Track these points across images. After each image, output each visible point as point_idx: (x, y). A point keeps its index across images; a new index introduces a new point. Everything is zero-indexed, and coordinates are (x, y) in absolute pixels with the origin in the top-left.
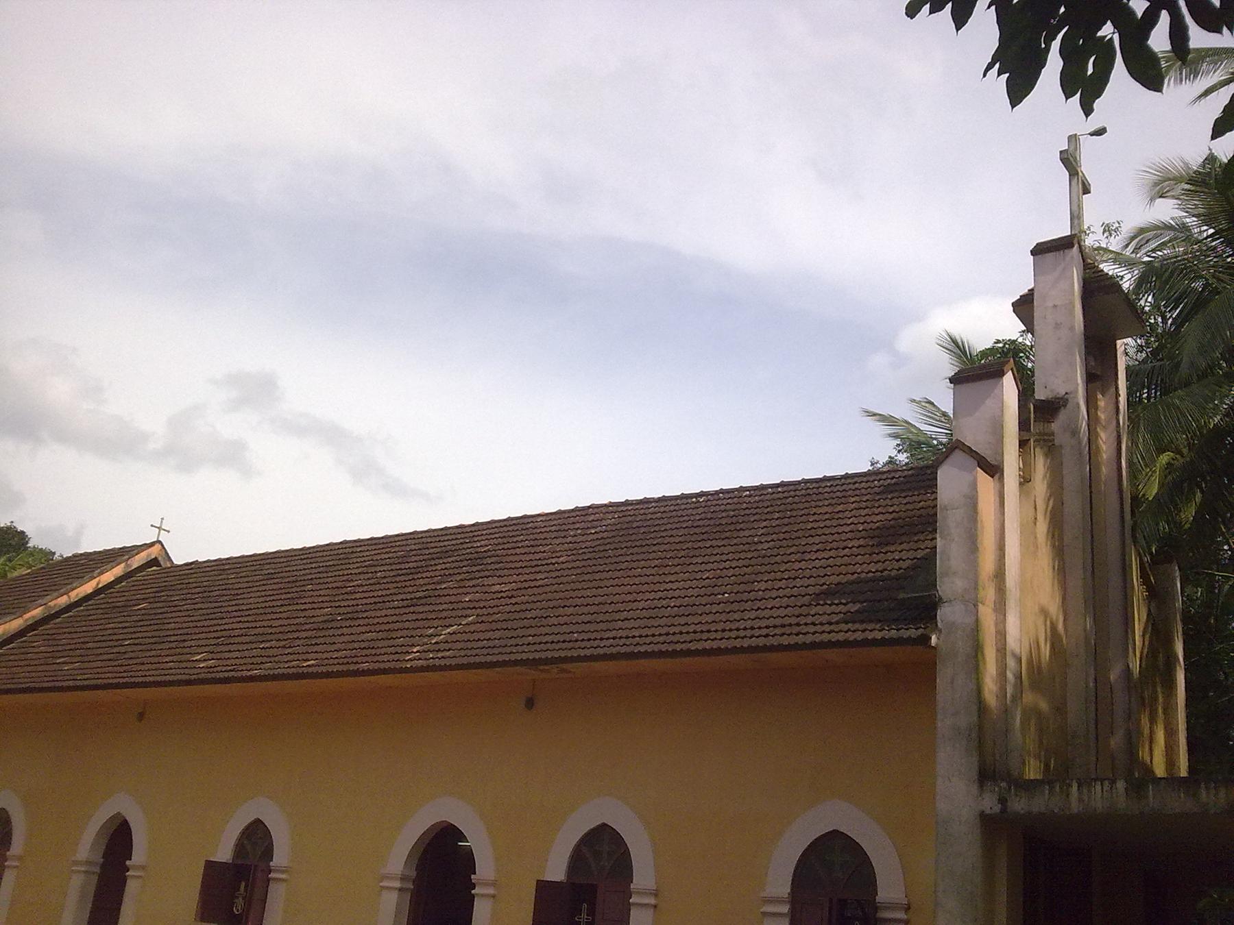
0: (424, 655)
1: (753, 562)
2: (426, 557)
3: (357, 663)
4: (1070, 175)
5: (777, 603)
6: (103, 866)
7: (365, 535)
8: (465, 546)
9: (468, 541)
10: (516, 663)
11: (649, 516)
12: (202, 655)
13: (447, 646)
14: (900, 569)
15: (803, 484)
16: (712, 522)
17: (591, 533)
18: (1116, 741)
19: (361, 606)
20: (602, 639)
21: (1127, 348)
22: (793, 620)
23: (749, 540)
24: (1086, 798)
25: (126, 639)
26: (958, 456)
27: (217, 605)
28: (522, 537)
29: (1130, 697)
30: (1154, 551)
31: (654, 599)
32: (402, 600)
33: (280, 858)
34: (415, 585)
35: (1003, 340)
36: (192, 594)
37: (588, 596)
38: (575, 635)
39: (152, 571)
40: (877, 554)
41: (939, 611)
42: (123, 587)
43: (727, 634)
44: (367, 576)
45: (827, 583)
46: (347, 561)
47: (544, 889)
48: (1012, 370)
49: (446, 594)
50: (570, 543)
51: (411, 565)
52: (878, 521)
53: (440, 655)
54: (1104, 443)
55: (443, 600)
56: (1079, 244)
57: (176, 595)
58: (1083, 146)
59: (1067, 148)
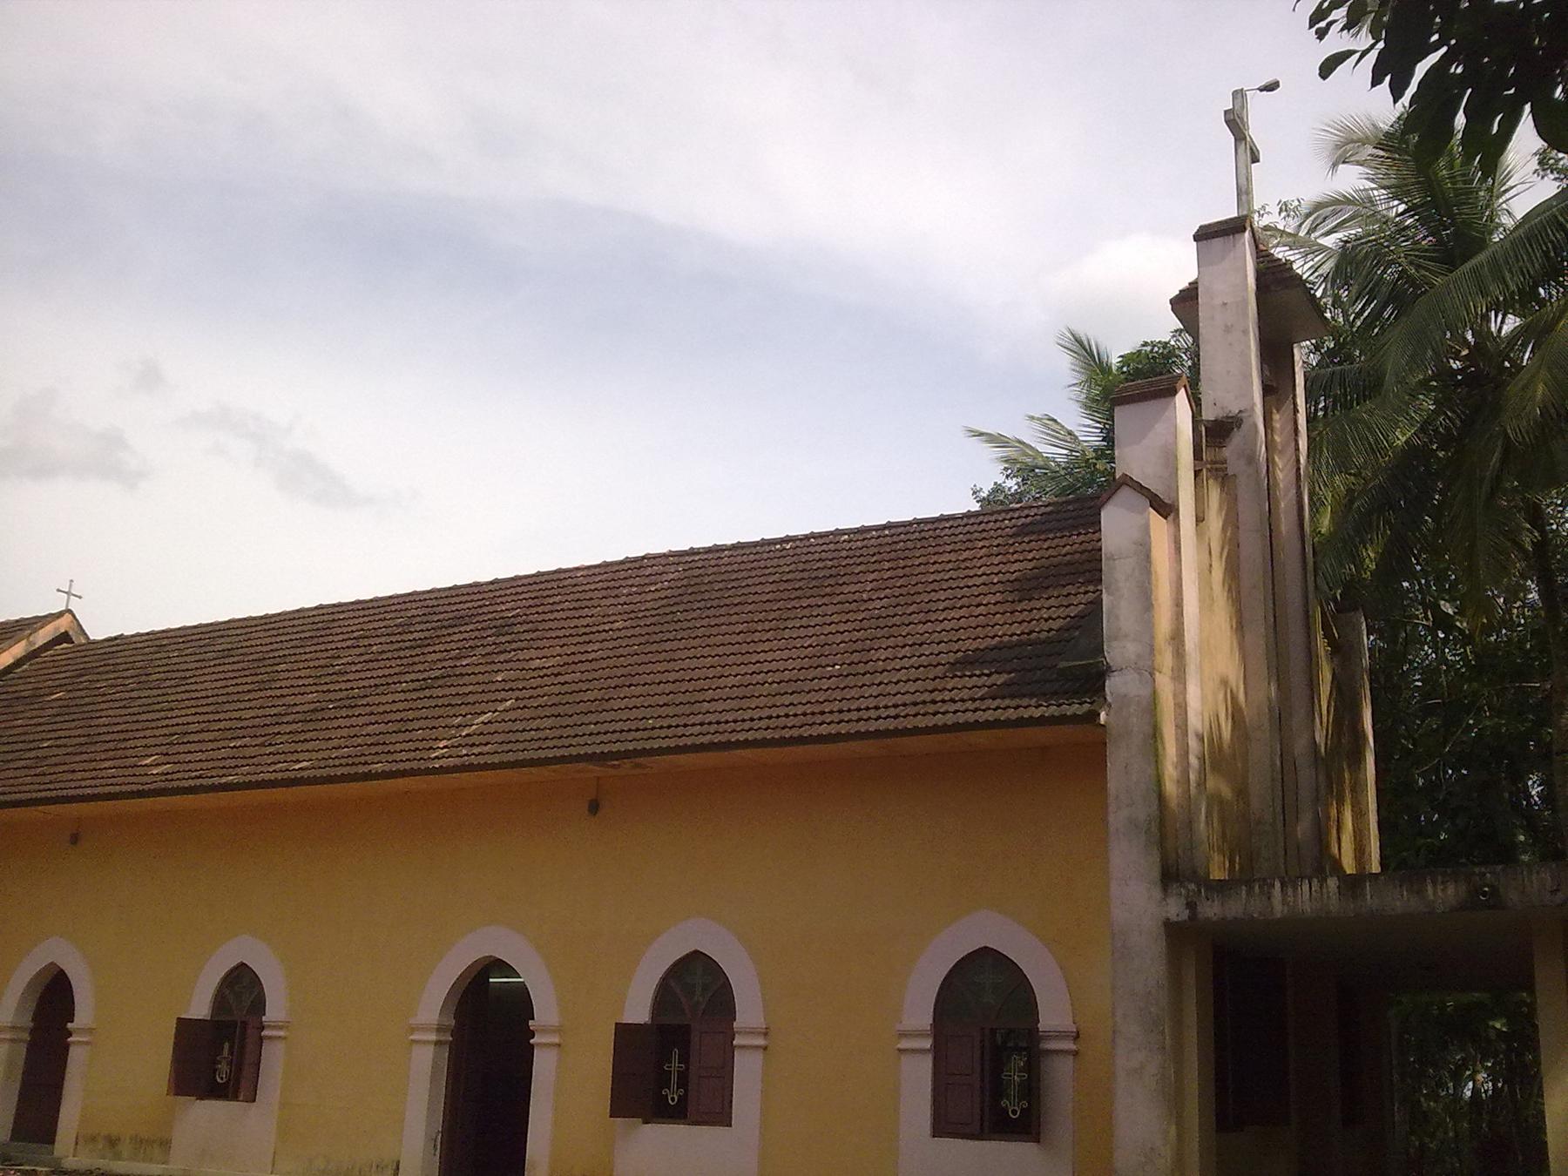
0: (454, 751)
1: (866, 624)
2: (434, 625)
3: (366, 763)
4: (1236, 140)
5: (902, 675)
6: (32, 1032)
7: (366, 595)
8: (485, 610)
9: (487, 603)
10: (578, 758)
11: (723, 569)
12: (153, 758)
13: (482, 739)
14: (1051, 630)
15: (915, 525)
16: (806, 575)
17: (650, 591)
18: (1303, 828)
19: (357, 690)
20: (685, 726)
21: (1303, 355)
22: (927, 697)
23: (856, 596)
24: (1291, 899)
25: (43, 739)
26: (1125, 494)
27: (160, 692)
28: (559, 597)
29: (1317, 774)
30: (1339, 597)
31: (746, 673)
32: (412, 681)
33: (275, 1010)
34: (426, 662)
35: (1152, 342)
36: (123, 678)
37: (659, 672)
38: (650, 722)
39: (62, 649)
40: (1020, 612)
41: (1107, 681)
42: (26, 670)
43: (846, 717)
44: (357, 651)
45: (963, 649)
46: (328, 632)
47: (625, 1033)
48: (1185, 387)
49: (470, 672)
50: (625, 603)
51: (416, 635)
52: (1015, 571)
53: (476, 750)
55: (466, 679)
56: (1251, 226)
57: (103, 680)
58: (1251, 106)
59: (1231, 107)
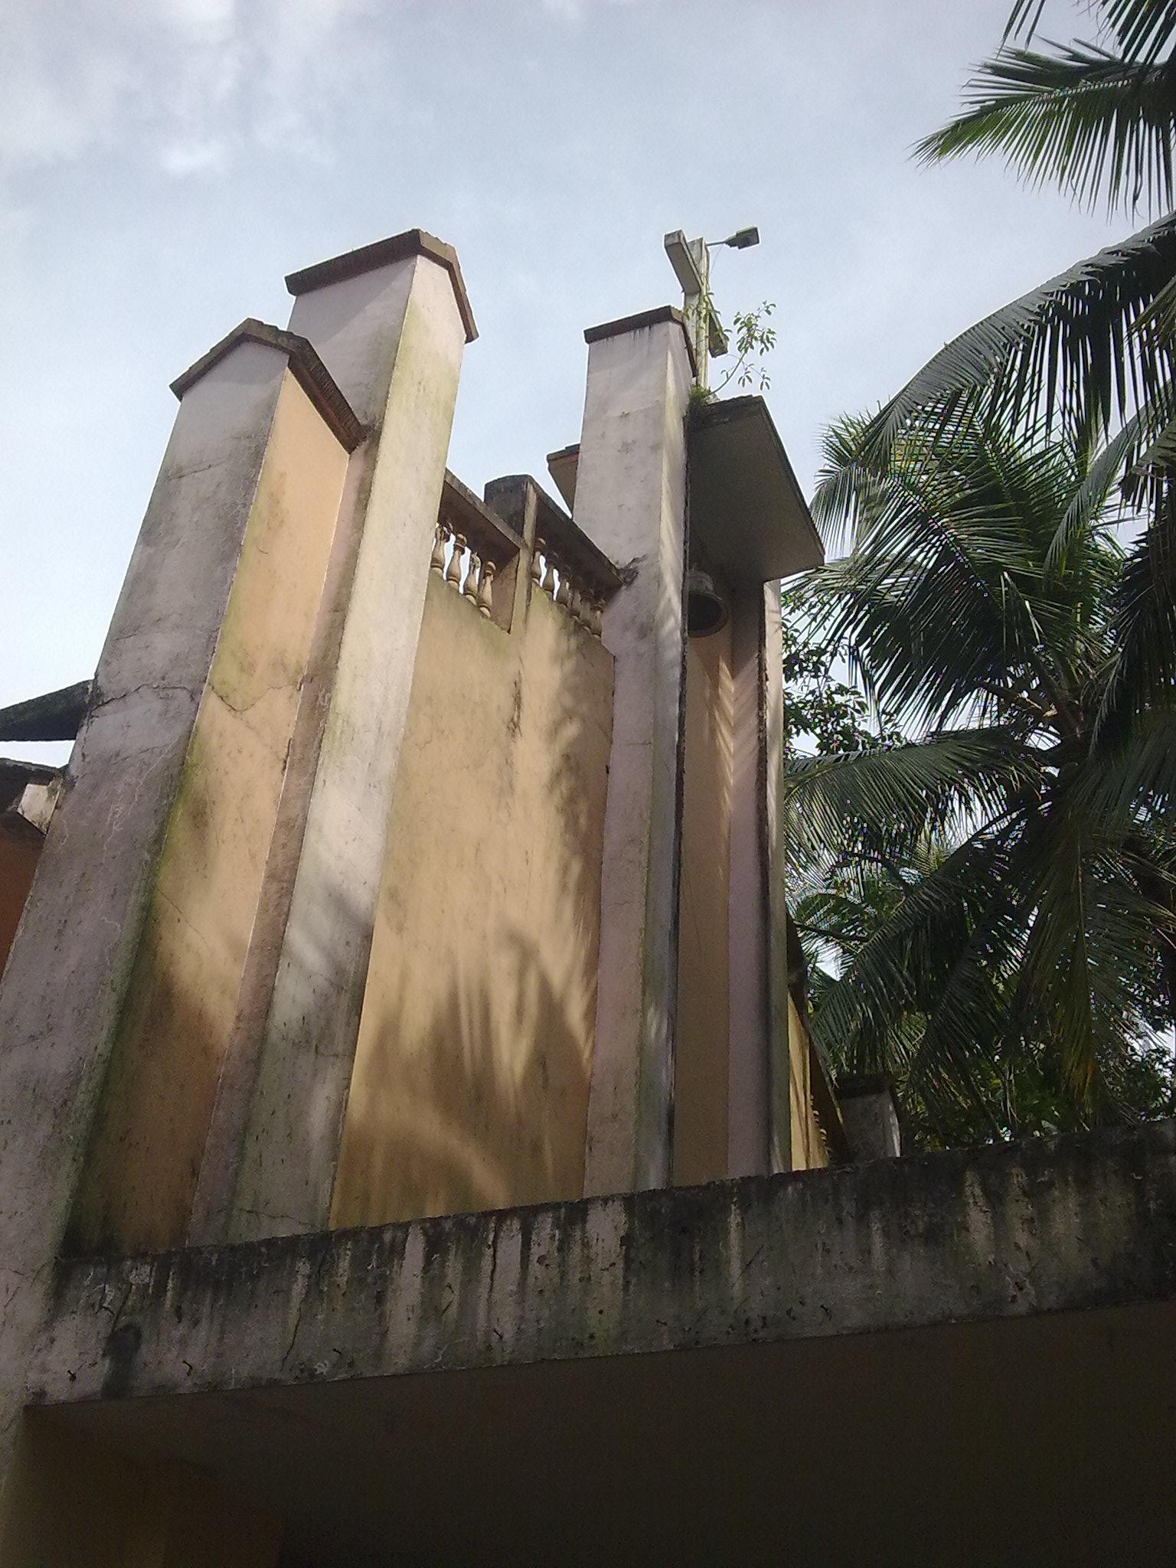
54: (733, 757)
